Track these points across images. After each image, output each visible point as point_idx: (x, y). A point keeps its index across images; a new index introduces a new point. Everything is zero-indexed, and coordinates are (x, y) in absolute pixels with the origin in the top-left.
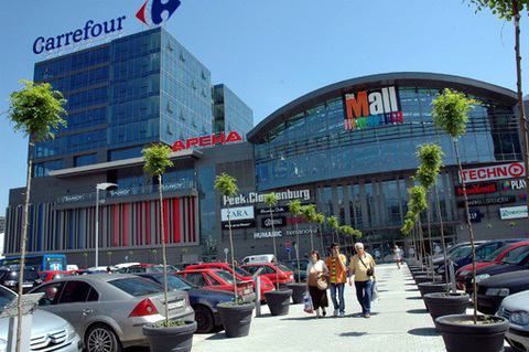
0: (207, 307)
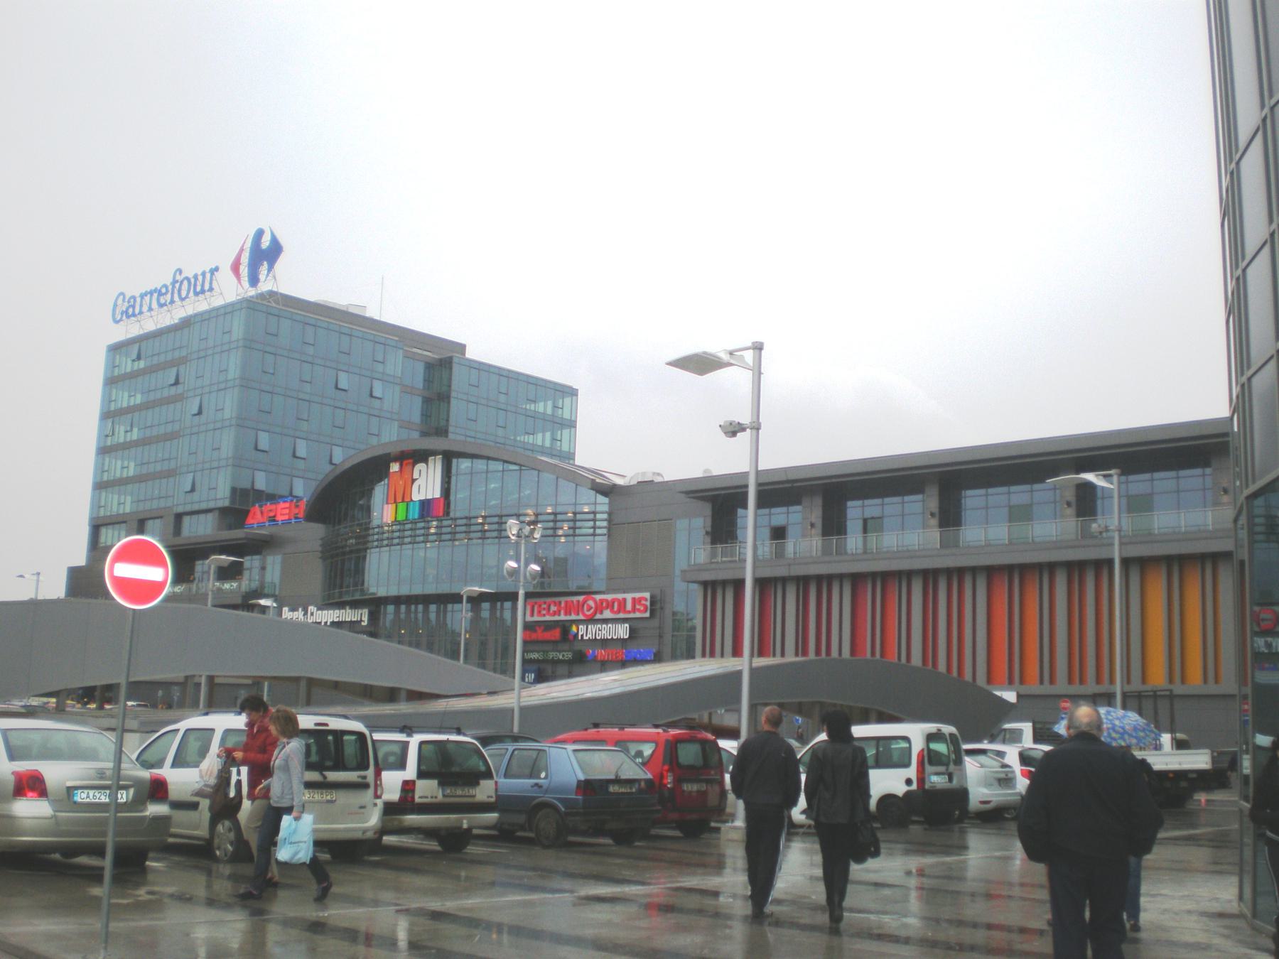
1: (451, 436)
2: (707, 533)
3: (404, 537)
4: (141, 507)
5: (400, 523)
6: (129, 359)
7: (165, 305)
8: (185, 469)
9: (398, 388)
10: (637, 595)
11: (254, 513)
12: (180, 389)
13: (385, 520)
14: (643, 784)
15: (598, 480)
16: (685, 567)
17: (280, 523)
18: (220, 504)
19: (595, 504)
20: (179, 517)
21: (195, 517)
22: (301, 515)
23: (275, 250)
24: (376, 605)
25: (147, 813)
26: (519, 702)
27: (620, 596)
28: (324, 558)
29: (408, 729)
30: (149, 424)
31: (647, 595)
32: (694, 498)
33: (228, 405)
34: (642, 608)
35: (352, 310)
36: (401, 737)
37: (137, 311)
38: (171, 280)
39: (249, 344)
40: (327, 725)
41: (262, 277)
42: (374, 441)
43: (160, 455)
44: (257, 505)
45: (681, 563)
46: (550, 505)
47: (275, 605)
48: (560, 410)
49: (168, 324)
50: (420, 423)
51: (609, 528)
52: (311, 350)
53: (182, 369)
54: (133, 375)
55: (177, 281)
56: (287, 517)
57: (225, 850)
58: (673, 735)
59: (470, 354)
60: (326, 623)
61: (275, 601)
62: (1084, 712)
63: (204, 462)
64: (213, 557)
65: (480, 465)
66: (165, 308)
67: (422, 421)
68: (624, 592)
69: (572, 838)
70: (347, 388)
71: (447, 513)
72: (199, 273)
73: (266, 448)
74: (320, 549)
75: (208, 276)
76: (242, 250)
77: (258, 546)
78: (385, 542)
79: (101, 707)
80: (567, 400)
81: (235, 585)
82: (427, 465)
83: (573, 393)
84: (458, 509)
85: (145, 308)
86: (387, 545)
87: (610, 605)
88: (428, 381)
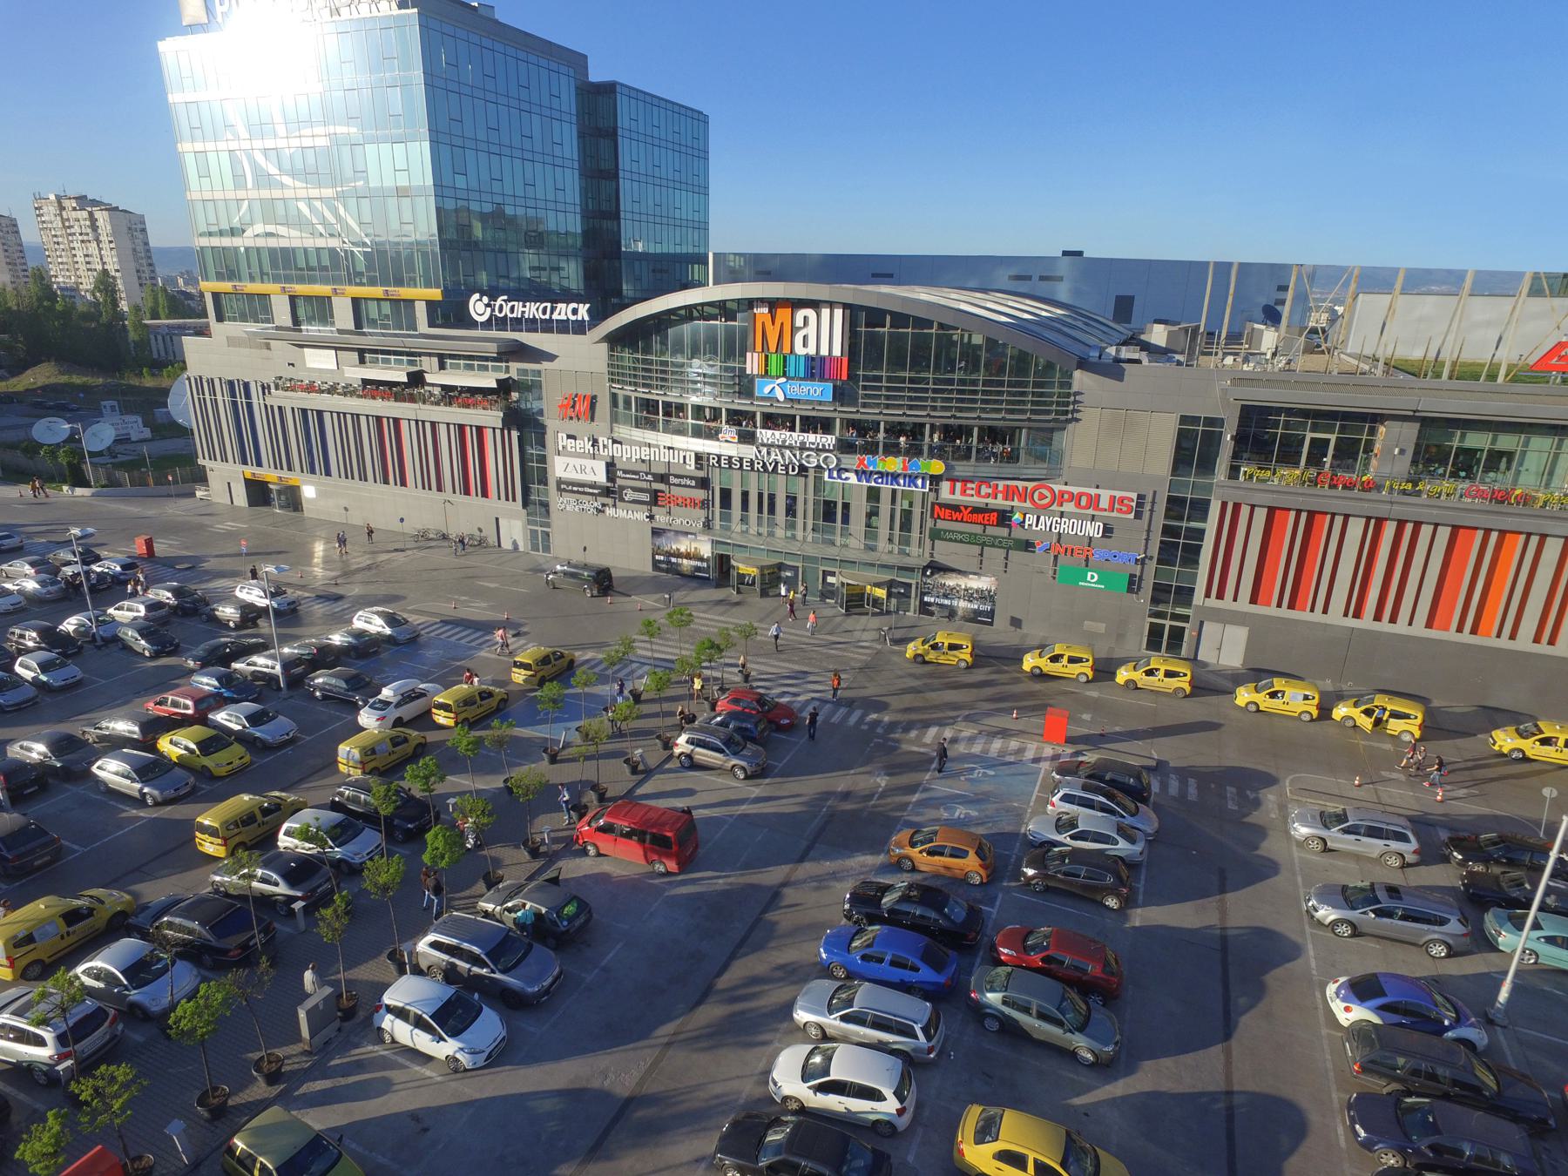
0: (113, 974)
10: (1118, 494)
31: (1134, 496)
62: (874, 716)
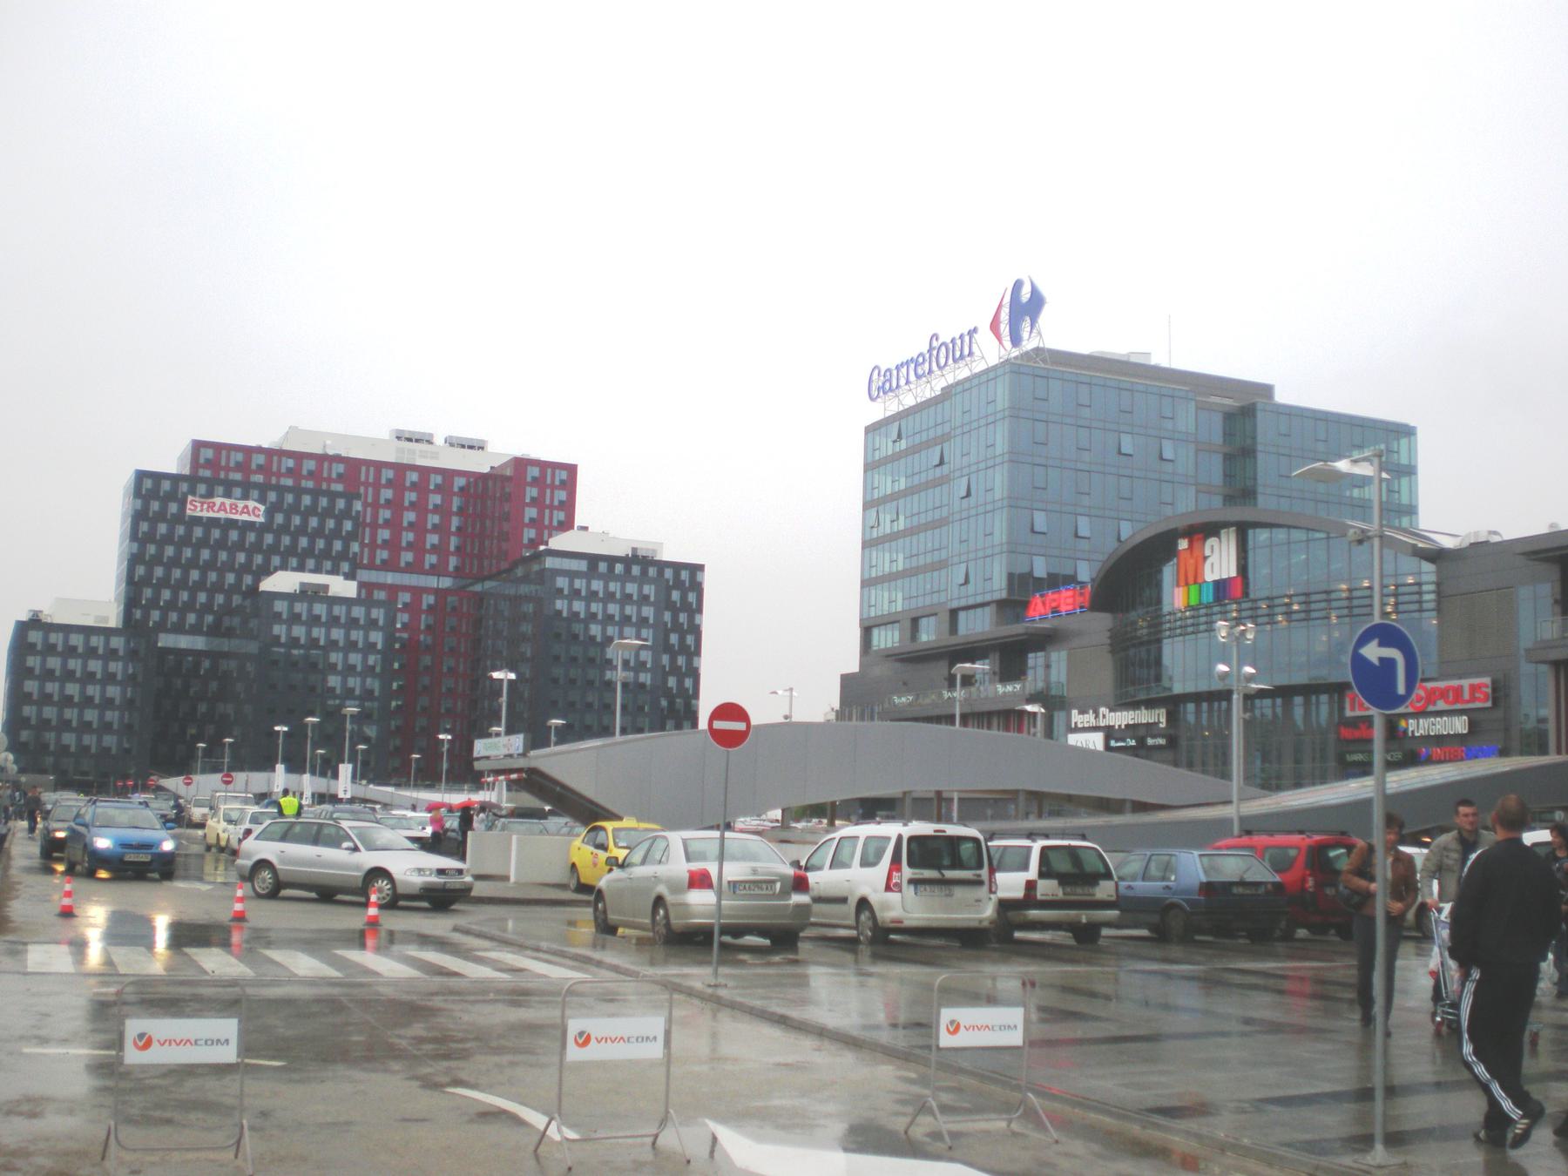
1: (1260, 499)
2: (1556, 602)
3: (1198, 625)
4: (914, 602)
5: (1193, 608)
6: (889, 440)
7: (923, 375)
8: (956, 559)
9: (1192, 447)
10: (1476, 681)
11: (1036, 605)
12: (945, 469)
13: (1176, 605)
14: (1269, 886)
15: (1420, 545)
16: (1530, 645)
17: (1064, 613)
18: (997, 596)
19: (1420, 573)
20: (954, 613)
21: (971, 612)
22: (1087, 604)
23: (1037, 302)
24: (1174, 704)
25: (791, 902)
26: (1238, 811)
27: (1455, 683)
28: (1113, 652)
29: (1031, 835)
30: (915, 511)
31: (1487, 680)
32: (1534, 560)
33: (999, 482)
34: (1482, 696)
35: (1133, 359)
36: (1026, 842)
37: (894, 385)
38: (928, 348)
39: (1015, 413)
40: (944, 831)
41: (1025, 335)
42: (1168, 511)
43: (930, 545)
44: (1038, 595)
45: (1526, 639)
46: (1366, 578)
47: (1043, 710)
48: (1396, 455)
49: (928, 396)
50: (1221, 484)
51: (1439, 601)
52: (1086, 412)
53: (946, 445)
54: (896, 457)
55: (934, 348)
56: (1070, 607)
57: (866, 936)
58: (1316, 841)
59: (1281, 397)
60: (1120, 726)
61: (1044, 707)
63: (976, 550)
64: (959, 665)
65: (1281, 535)
66: (924, 379)
67: (1225, 482)
68: (1460, 678)
69: (1198, 938)
70: (1131, 453)
71: (1246, 594)
72: (958, 337)
73: (1044, 529)
74: (1109, 641)
75: (967, 339)
76: (1000, 306)
77: (1043, 640)
78: (1202, 627)
79: (831, 823)
80: (1404, 442)
81: (1018, 686)
82: (1219, 538)
83: (1407, 432)
84: (1259, 587)
85: (902, 382)
86: (1181, 635)
87: (1443, 694)
88: (1228, 434)
